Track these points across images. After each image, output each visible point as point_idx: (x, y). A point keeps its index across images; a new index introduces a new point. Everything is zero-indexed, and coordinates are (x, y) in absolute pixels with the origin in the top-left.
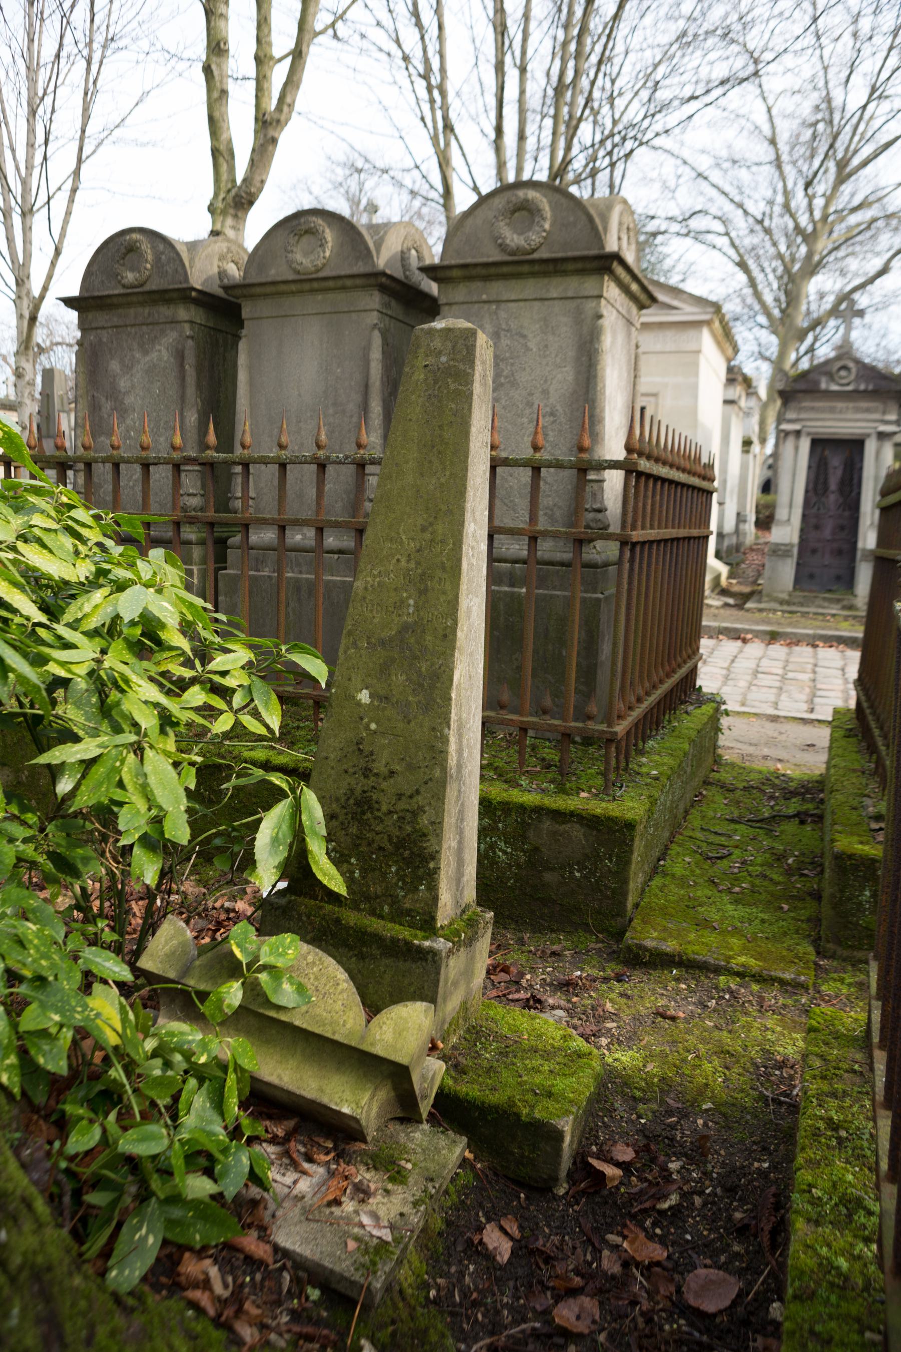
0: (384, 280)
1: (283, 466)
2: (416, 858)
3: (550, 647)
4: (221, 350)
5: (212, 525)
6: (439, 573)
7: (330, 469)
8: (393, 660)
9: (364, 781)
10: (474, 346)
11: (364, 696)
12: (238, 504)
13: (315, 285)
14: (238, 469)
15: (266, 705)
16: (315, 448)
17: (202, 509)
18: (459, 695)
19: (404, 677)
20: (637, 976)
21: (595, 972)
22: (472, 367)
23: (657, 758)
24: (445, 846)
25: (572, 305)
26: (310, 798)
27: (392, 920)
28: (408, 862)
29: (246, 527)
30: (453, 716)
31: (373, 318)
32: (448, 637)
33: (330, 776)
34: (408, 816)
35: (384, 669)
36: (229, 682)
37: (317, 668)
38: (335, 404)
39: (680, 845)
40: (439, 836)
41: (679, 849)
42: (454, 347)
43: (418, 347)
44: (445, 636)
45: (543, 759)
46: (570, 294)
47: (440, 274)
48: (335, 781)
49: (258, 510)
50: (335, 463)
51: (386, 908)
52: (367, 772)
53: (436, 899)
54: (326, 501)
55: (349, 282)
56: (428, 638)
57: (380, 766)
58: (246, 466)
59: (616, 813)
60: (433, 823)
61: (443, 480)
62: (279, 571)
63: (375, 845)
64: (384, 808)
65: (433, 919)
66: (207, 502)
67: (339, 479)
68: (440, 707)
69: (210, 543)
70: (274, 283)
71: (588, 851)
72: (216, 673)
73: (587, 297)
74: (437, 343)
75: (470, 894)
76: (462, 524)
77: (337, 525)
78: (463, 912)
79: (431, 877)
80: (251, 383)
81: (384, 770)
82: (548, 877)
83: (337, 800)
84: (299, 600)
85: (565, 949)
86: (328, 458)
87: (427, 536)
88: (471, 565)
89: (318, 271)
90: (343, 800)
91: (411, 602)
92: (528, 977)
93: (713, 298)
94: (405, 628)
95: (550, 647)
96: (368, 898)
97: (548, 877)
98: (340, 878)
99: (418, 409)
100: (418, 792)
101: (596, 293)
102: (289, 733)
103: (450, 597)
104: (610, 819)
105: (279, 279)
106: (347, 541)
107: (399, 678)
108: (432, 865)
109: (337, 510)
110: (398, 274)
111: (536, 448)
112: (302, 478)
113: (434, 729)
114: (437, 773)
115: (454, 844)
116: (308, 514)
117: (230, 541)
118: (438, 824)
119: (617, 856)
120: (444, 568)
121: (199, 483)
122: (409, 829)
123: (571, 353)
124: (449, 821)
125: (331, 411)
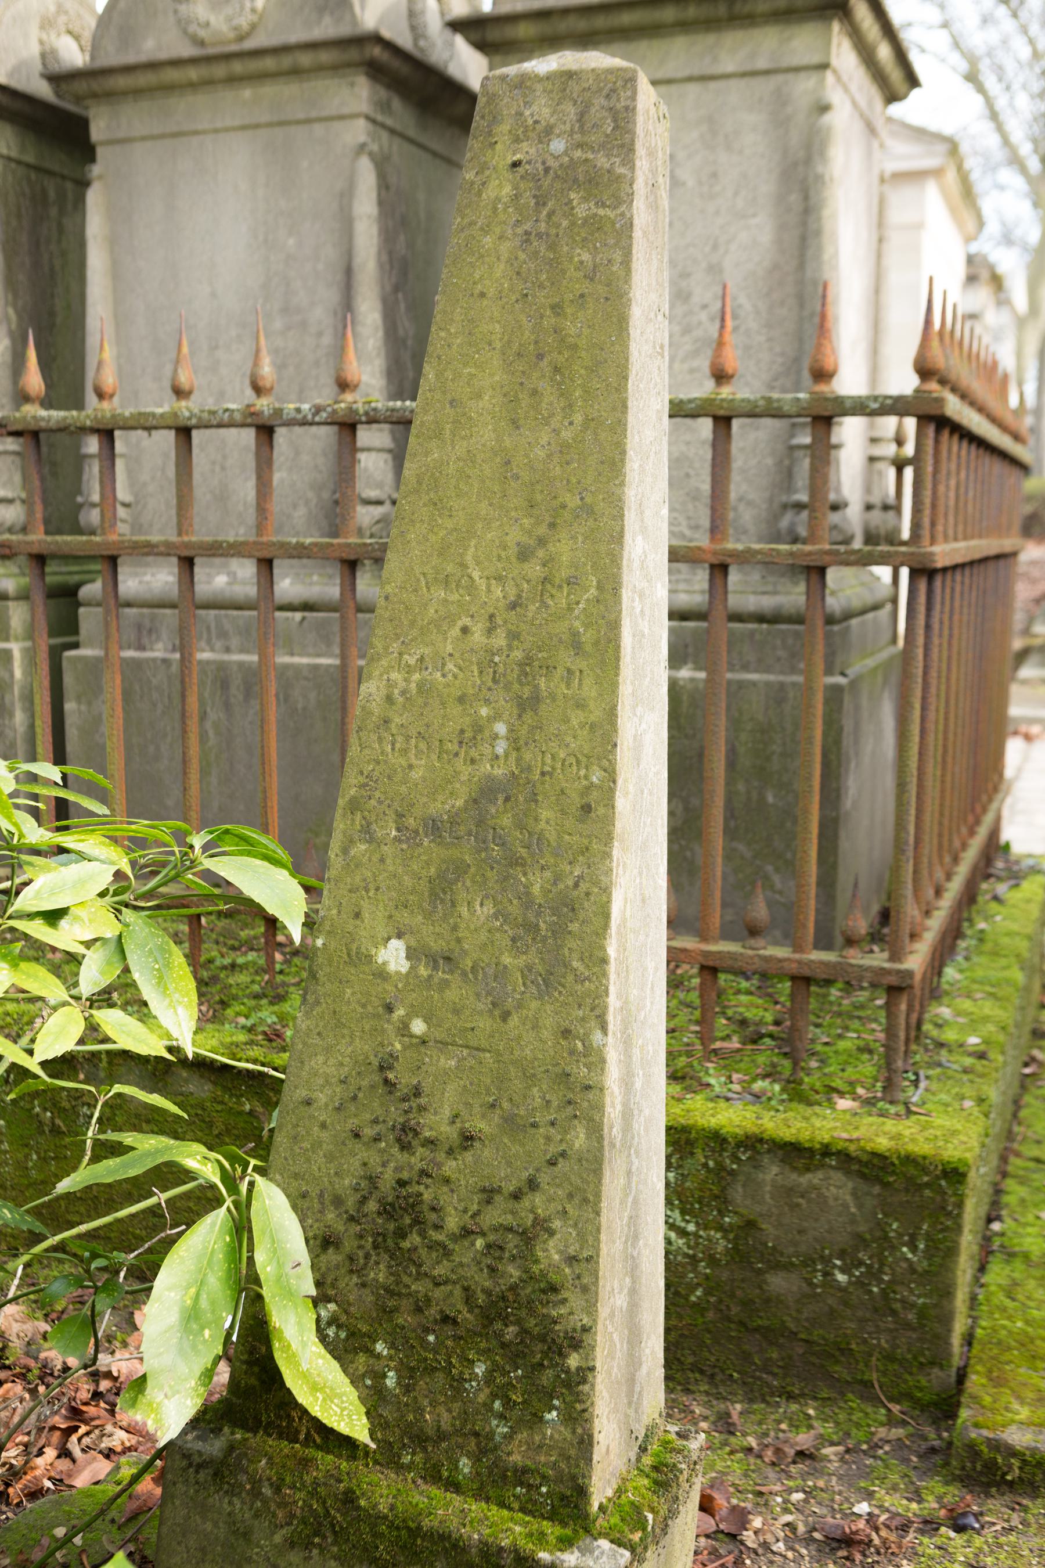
0: (377, 51)
1: (184, 433)
2: (534, 1346)
3: (741, 787)
4: (54, 212)
5: (40, 560)
6: (565, 658)
7: (281, 435)
8: (461, 869)
9: (403, 1157)
10: (631, 110)
11: (394, 956)
12: (94, 516)
13: (238, 67)
14: (92, 445)
15: (161, 981)
16: (249, 392)
17: (24, 530)
18: (622, 948)
19: (489, 909)
20: (996, 1512)
21: (898, 1504)
22: (629, 161)
23: (967, 1005)
24: (603, 1312)
25: (764, 86)
26: (273, 1206)
27: (481, 1494)
28: (515, 1354)
29: (113, 561)
30: (613, 1001)
31: (358, 131)
32: (594, 810)
33: (317, 1145)
34: (512, 1242)
35: (441, 891)
36: (65, 937)
37: (275, 890)
38: (285, 310)
39: (1023, 1181)
40: (589, 1291)
41: (1022, 1191)
42: (581, 116)
43: (495, 120)
44: (587, 809)
45: (743, 1023)
46: (762, 64)
47: (493, 34)
48: (330, 1157)
49: (137, 526)
50: (290, 423)
51: (465, 1465)
52: (406, 1136)
53: (586, 1443)
54: (277, 505)
55: (305, 59)
56: (545, 814)
57: (437, 1123)
58: (107, 435)
59: (921, 1147)
60: (572, 1260)
61: (567, 434)
62: (184, 647)
63: (433, 1312)
64: (452, 1222)
65: (582, 1492)
66: (30, 513)
67: (302, 454)
68: (580, 980)
69: (38, 598)
70: (153, 66)
71: (862, 1228)
72: (31, 916)
73: (797, 69)
74: (541, 109)
75: (654, 1394)
76: (618, 538)
77: (299, 552)
78: (643, 1449)
79: (574, 1388)
80: (116, 273)
81: (448, 1132)
82: (777, 1282)
83: (338, 1201)
84: (227, 706)
85: (825, 1440)
86: (278, 412)
87: (535, 569)
88: (638, 635)
89: (241, 38)
90: (351, 1202)
91: (501, 728)
92: (757, 1522)
93: (948, 130)
94: (488, 791)
95: (741, 787)
96: (420, 1440)
97: (777, 1282)
98: (351, 1394)
99: (500, 269)
100: (532, 1184)
101: (816, 59)
102: (215, 979)
103: (596, 714)
104: (909, 1160)
105: (163, 55)
106: (324, 585)
107: (477, 913)
108: (573, 1361)
109: (297, 521)
110: (404, 40)
111: (721, 376)
112: (225, 457)
113: (566, 1033)
114: (579, 1139)
115: (621, 1301)
116: (239, 530)
117: (84, 592)
118: (584, 1261)
119: (928, 1237)
120: (576, 645)
121: (17, 478)
122: (514, 1272)
123: (767, 187)
124: (610, 1250)
125: (278, 324)
